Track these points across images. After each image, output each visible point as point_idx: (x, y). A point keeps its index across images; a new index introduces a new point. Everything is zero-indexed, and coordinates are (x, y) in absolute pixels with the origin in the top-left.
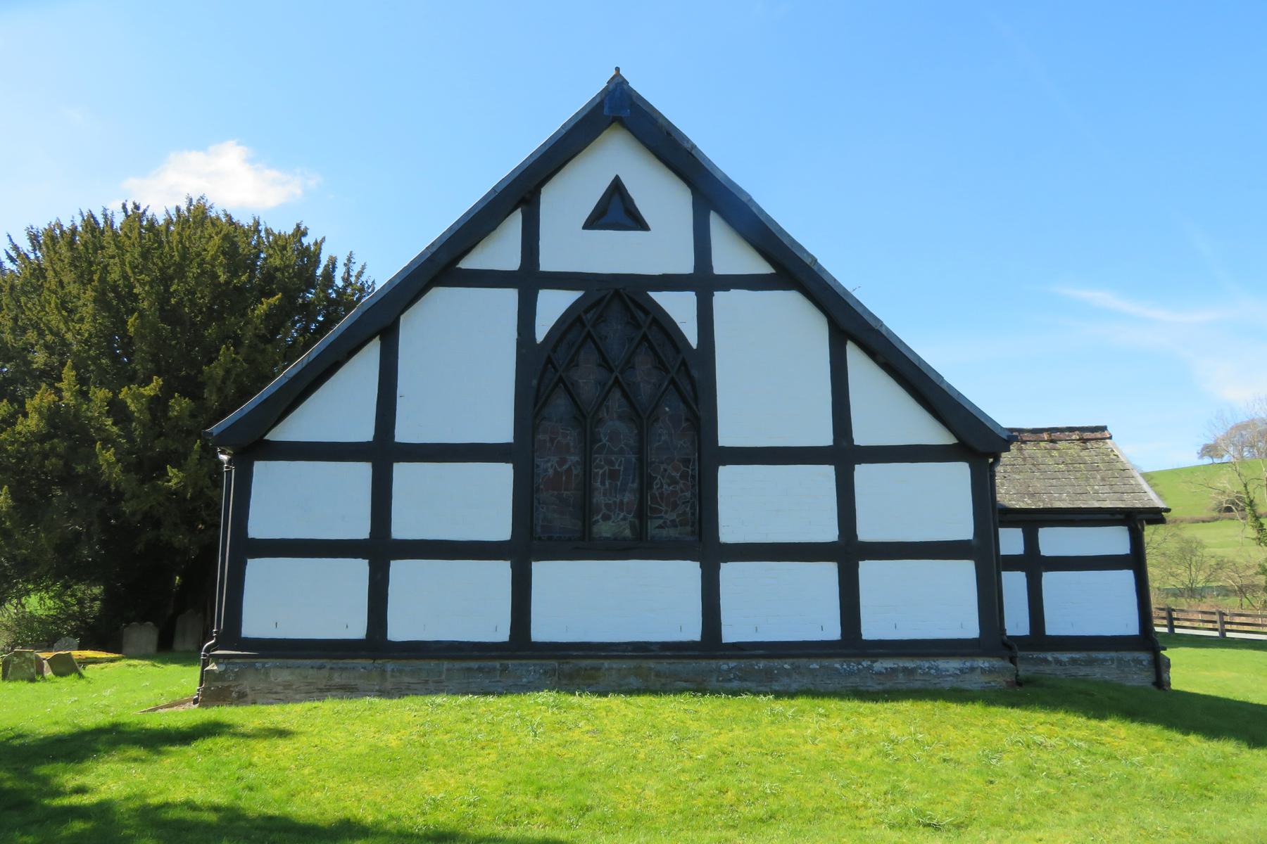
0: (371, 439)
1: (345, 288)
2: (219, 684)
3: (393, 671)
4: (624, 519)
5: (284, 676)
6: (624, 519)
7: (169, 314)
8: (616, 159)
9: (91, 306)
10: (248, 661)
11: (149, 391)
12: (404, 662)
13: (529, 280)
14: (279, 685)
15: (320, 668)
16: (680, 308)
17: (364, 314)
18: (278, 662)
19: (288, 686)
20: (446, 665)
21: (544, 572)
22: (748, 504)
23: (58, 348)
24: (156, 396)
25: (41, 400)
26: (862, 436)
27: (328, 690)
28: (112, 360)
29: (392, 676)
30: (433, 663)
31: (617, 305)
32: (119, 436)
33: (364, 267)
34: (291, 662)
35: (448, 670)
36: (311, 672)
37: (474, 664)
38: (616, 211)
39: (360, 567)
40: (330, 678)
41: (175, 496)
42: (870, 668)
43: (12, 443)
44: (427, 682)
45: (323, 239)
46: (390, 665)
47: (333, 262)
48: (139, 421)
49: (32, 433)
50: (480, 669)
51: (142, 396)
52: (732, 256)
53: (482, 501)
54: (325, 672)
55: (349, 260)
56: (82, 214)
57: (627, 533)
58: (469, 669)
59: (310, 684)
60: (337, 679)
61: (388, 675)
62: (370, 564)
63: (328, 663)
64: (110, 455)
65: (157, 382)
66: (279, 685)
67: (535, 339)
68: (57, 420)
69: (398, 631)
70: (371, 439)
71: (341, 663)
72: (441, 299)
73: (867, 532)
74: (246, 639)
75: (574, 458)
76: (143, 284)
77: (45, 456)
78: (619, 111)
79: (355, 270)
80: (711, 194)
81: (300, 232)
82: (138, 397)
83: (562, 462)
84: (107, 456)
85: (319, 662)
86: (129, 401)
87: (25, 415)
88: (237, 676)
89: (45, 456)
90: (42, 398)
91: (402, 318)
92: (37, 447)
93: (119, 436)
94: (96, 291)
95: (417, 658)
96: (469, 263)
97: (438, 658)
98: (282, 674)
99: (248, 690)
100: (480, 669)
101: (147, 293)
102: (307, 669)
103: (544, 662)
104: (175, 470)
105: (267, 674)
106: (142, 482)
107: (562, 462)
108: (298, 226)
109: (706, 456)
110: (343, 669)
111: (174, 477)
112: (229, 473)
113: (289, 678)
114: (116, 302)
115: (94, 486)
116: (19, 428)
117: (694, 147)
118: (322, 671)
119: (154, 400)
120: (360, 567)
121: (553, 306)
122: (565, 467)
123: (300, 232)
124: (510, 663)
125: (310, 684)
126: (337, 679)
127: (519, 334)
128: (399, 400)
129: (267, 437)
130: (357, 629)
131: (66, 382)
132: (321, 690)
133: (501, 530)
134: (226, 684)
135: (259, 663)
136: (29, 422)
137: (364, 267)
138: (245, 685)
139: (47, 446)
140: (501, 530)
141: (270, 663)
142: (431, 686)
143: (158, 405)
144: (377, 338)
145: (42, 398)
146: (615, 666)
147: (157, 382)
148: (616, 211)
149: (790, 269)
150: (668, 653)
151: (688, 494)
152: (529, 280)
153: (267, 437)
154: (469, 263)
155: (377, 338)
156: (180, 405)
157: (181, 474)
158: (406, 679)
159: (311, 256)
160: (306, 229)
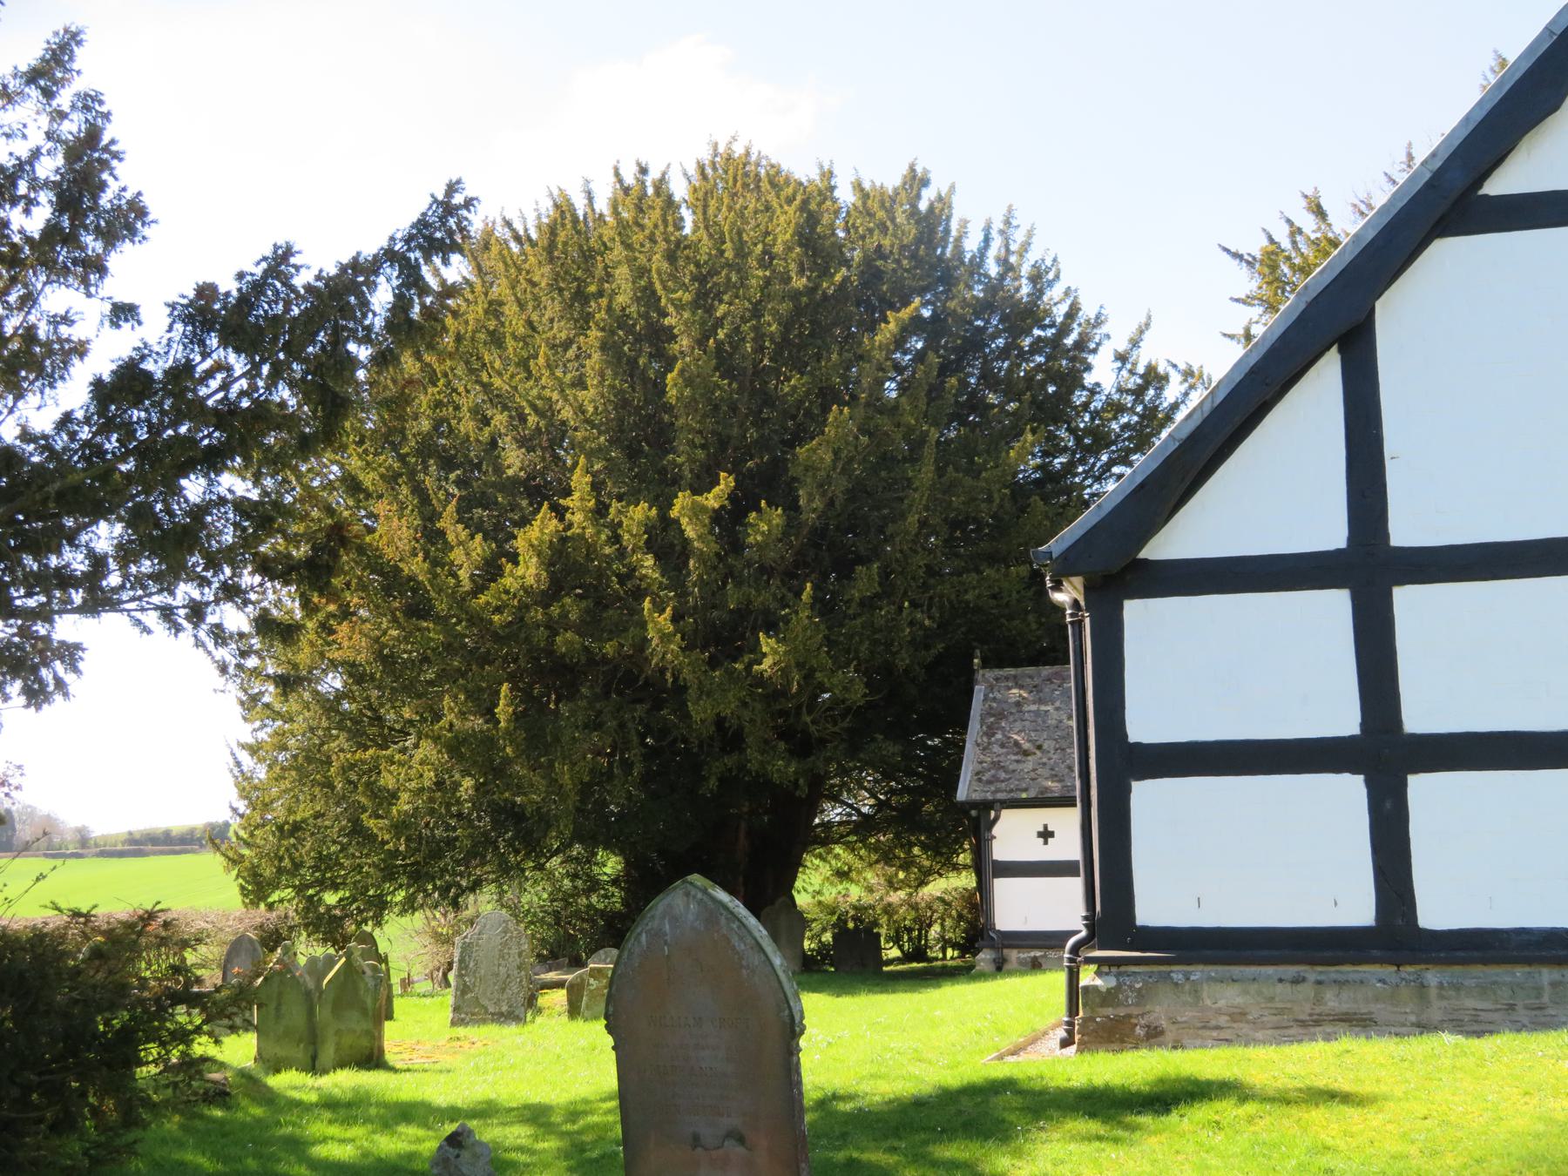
0: (1341, 543)
1: (1002, 277)
3: (1441, 986)
7: (724, 361)
9: (596, 356)
10: (1156, 968)
11: (713, 499)
12: (1457, 969)
15: (1298, 981)
17: (1310, 305)
18: (1214, 970)
19: (1238, 1015)
23: (549, 438)
24: (722, 507)
25: (541, 531)
26: (1329, 530)
27: (1317, 1023)
28: (642, 447)
29: (1441, 997)
30: (1520, 972)
32: (661, 587)
33: (1030, 234)
34: (1236, 970)
35: (1554, 985)
40: (1318, 1000)
41: (771, 693)
43: (498, 610)
44: (1512, 1007)
45: (952, 188)
46: (1433, 976)
47: (964, 224)
48: (702, 558)
49: (527, 590)
51: (704, 509)
54: (1307, 990)
55: (1007, 222)
56: (551, 194)
59: (1280, 1012)
60: (1333, 1001)
61: (1433, 992)
62: (1368, 783)
63: (1312, 973)
64: (664, 620)
65: (726, 482)
66: (1219, 1012)
68: (565, 563)
70: (1341, 543)
71: (1333, 972)
72: (1451, 260)
74: (1145, 929)
76: (679, 307)
77: (552, 628)
79: (1018, 237)
81: (916, 181)
82: (697, 511)
84: (659, 621)
85: (1291, 971)
86: (684, 521)
87: (514, 558)
89: (552, 628)
90: (543, 527)
91: (1379, 305)
92: (537, 614)
93: (661, 587)
94: (603, 329)
95: (1485, 962)
96: (1501, 184)
97: (1528, 961)
98: (1224, 991)
99: (1164, 1023)
101: (686, 323)
102: (1267, 984)
104: (772, 641)
105: (1196, 993)
106: (713, 663)
108: (912, 169)
111: (771, 654)
112: (1078, 625)
113: (1239, 1000)
114: (640, 343)
115: (633, 682)
116: (507, 581)
118: (1300, 987)
119: (717, 516)
123: (916, 181)
125: (1280, 1012)
129: (1143, 554)
130: (1357, 907)
131: (576, 495)
132: (1303, 1024)
134: (1122, 1012)
135: (1177, 972)
136: (520, 571)
137: (1030, 234)
138: (1159, 1011)
139: (555, 610)
141: (1198, 972)
142: (1522, 1015)
143: (729, 521)
144: (1334, 349)
145: (543, 527)
147: (726, 482)
153: (1143, 554)
154: (1501, 184)
155: (1334, 349)
156: (769, 523)
157: (782, 649)
158: (1470, 1003)
159: (932, 224)
160: (926, 171)
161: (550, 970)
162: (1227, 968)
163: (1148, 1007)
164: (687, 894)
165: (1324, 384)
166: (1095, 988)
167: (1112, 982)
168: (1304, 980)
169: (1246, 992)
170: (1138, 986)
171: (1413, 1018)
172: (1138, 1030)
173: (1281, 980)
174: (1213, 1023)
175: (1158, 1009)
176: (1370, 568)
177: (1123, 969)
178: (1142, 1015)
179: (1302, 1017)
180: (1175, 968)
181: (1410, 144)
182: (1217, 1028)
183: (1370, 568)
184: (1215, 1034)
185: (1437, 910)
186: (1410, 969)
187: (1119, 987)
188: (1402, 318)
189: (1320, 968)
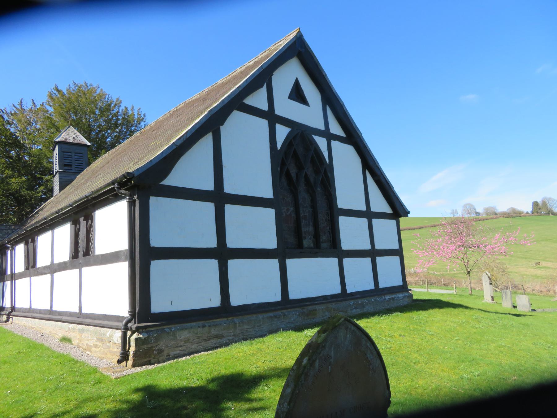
2: (145, 347)
3: (239, 323)
4: (310, 239)
5: (184, 335)
6: (310, 239)
8: (292, 72)
13: (271, 117)
14: (181, 341)
15: (204, 326)
16: (321, 142)
17: (212, 116)
18: (178, 326)
20: (260, 316)
21: (291, 263)
22: (352, 233)
29: (239, 326)
30: (254, 316)
31: (301, 135)
34: (185, 325)
36: (199, 329)
37: (271, 314)
38: (297, 94)
39: (232, 264)
40: (210, 332)
42: (385, 299)
44: (254, 326)
46: (236, 320)
50: (275, 317)
52: (336, 129)
53: (256, 227)
54: (207, 329)
57: (312, 245)
58: (271, 317)
59: (199, 337)
60: (213, 332)
61: (238, 325)
63: (207, 323)
66: (181, 341)
67: (277, 148)
69: (236, 300)
72: (237, 116)
73: (232, 242)
75: (292, 209)
78: (299, 50)
80: (330, 99)
83: (288, 210)
85: (201, 323)
88: (157, 339)
98: (184, 334)
100: (275, 317)
103: (296, 309)
105: (175, 335)
107: (288, 210)
109: (333, 213)
110: (215, 326)
113: (188, 335)
117: (326, 75)
120: (232, 264)
121: (282, 132)
122: (289, 212)
124: (284, 311)
126: (213, 332)
127: (270, 144)
128: (224, 168)
130: (215, 302)
133: (271, 243)
134: (149, 346)
140: (271, 243)
141: (173, 327)
146: (320, 308)
148: (297, 94)
149: (352, 137)
150: (334, 300)
151: (328, 228)
152: (271, 117)
158: (246, 327)
161: (196, 407)
162: (182, 325)
163: (158, 343)
164: (347, 328)
165: (207, 141)
166: (140, 338)
167: (146, 336)
168: (205, 326)
169: (190, 332)
170: (155, 335)
171: (232, 334)
172: (155, 352)
173: (199, 327)
174: (179, 345)
175: (162, 343)
176: (219, 198)
177: (147, 330)
178: (156, 346)
179: (205, 338)
180: (165, 327)
181: (22, 99)
182: (181, 346)
183: (219, 198)
184: (180, 349)
185: (236, 300)
186: (230, 319)
187: (148, 337)
188: (226, 130)
189: (207, 321)
